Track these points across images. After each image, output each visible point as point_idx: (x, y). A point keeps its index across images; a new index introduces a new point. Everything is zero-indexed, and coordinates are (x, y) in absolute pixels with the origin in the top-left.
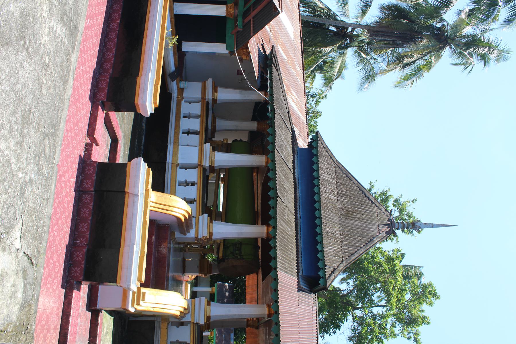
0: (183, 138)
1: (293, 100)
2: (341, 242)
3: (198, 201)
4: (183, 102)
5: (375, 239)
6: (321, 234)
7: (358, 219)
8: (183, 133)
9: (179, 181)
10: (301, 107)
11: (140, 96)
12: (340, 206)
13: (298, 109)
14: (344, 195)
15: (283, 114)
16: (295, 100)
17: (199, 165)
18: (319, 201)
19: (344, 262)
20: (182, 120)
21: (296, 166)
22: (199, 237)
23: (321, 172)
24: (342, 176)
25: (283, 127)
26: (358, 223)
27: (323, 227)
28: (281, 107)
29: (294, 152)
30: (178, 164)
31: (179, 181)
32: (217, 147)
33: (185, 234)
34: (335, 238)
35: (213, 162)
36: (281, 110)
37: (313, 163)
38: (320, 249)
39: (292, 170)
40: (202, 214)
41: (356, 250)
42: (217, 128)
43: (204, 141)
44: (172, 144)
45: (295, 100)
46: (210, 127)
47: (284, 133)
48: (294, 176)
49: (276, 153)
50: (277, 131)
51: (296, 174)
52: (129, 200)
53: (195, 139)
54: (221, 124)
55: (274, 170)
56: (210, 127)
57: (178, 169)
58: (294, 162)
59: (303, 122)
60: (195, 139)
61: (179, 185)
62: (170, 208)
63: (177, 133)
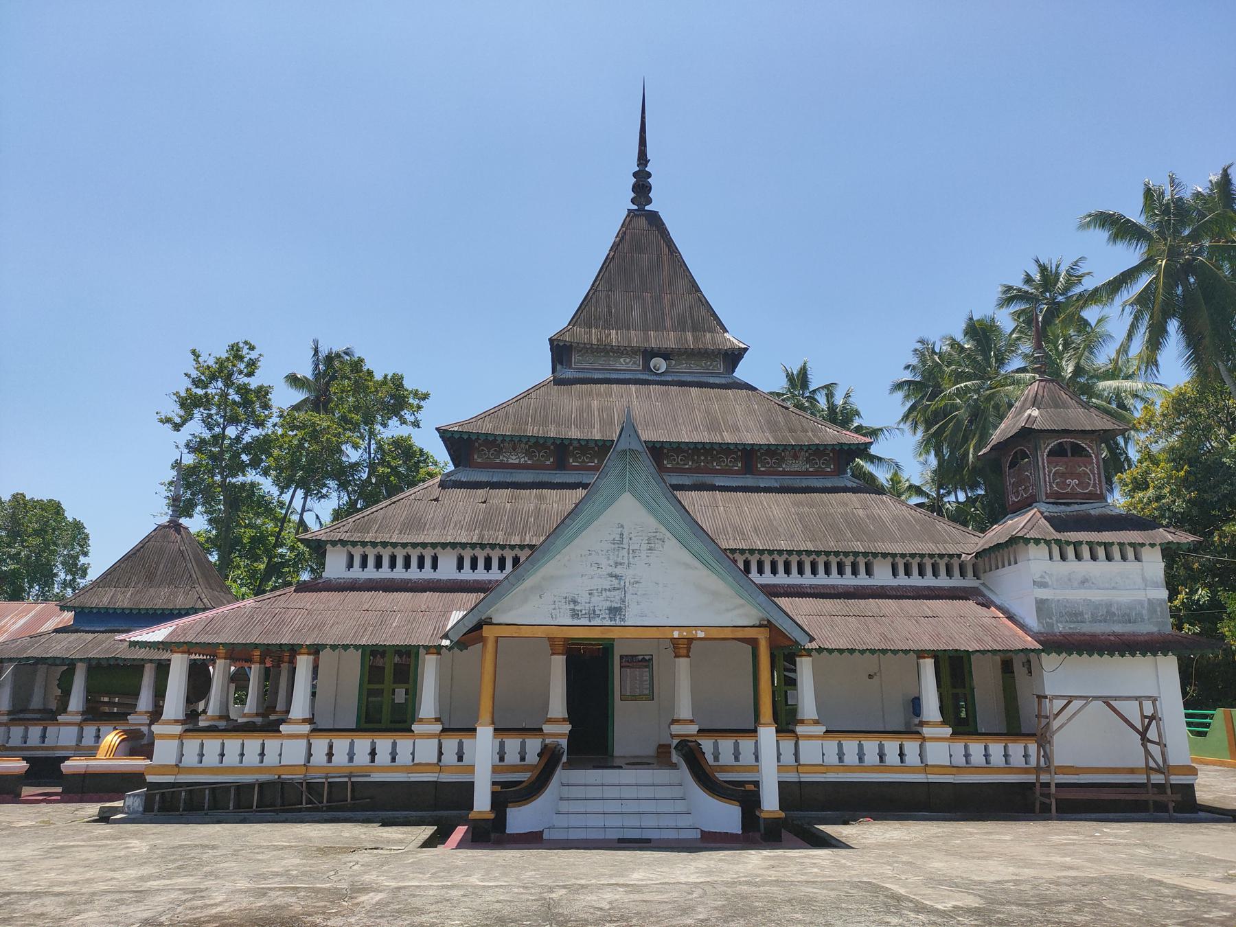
0: (48, 743)
1: (14, 623)
2: (175, 587)
3: (115, 725)
4: (7, 745)
5: (181, 548)
6: (163, 609)
7: (157, 565)
8: (44, 742)
9: (714, 762)
10: (22, 612)
11: (13, 771)
12: (140, 585)
13: (26, 615)
14: (129, 579)
15: (32, 646)
16: (13, 620)
17: (80, 726)
18: (131, 609)
19: (196, 586)
20: (28, 744)
21: (92, 629)
22: (148, 722)
23: (101, 605)
24: (110, 580)
25: (47, 645)
26: (161, 566)
27: (157, 607)
28: (25, 649)
29: (77, 631)
30: (77, 745)
31: (714, 762)
32: (63, 708)
33: (145, 735)
34: (171, 594)
35: (77, 713)
36: (28, 649)
37: (91, 612)
38: (177, 611)
39: (96, 635)
40: (128, 720)
41: (187, 572)
42: (42, 707)
43: (55, 722)
44: (56, 752)
45: (13, 620)
46: (38, 716)
47: (54, 645)
48: (103, 632)
49: (73, 657)
50: (51, 655)
51: (101, 629)
52: (91, 770)
53: (51, 730)
54: (36, 702)
55: (90, 659)
56: (38, 716)
57: (83, 744)
58: (87, 632)
59: (42, 609)
60: (51, 730)
61: (739, 761)
62: (111, 747)
63: (47, 748)
